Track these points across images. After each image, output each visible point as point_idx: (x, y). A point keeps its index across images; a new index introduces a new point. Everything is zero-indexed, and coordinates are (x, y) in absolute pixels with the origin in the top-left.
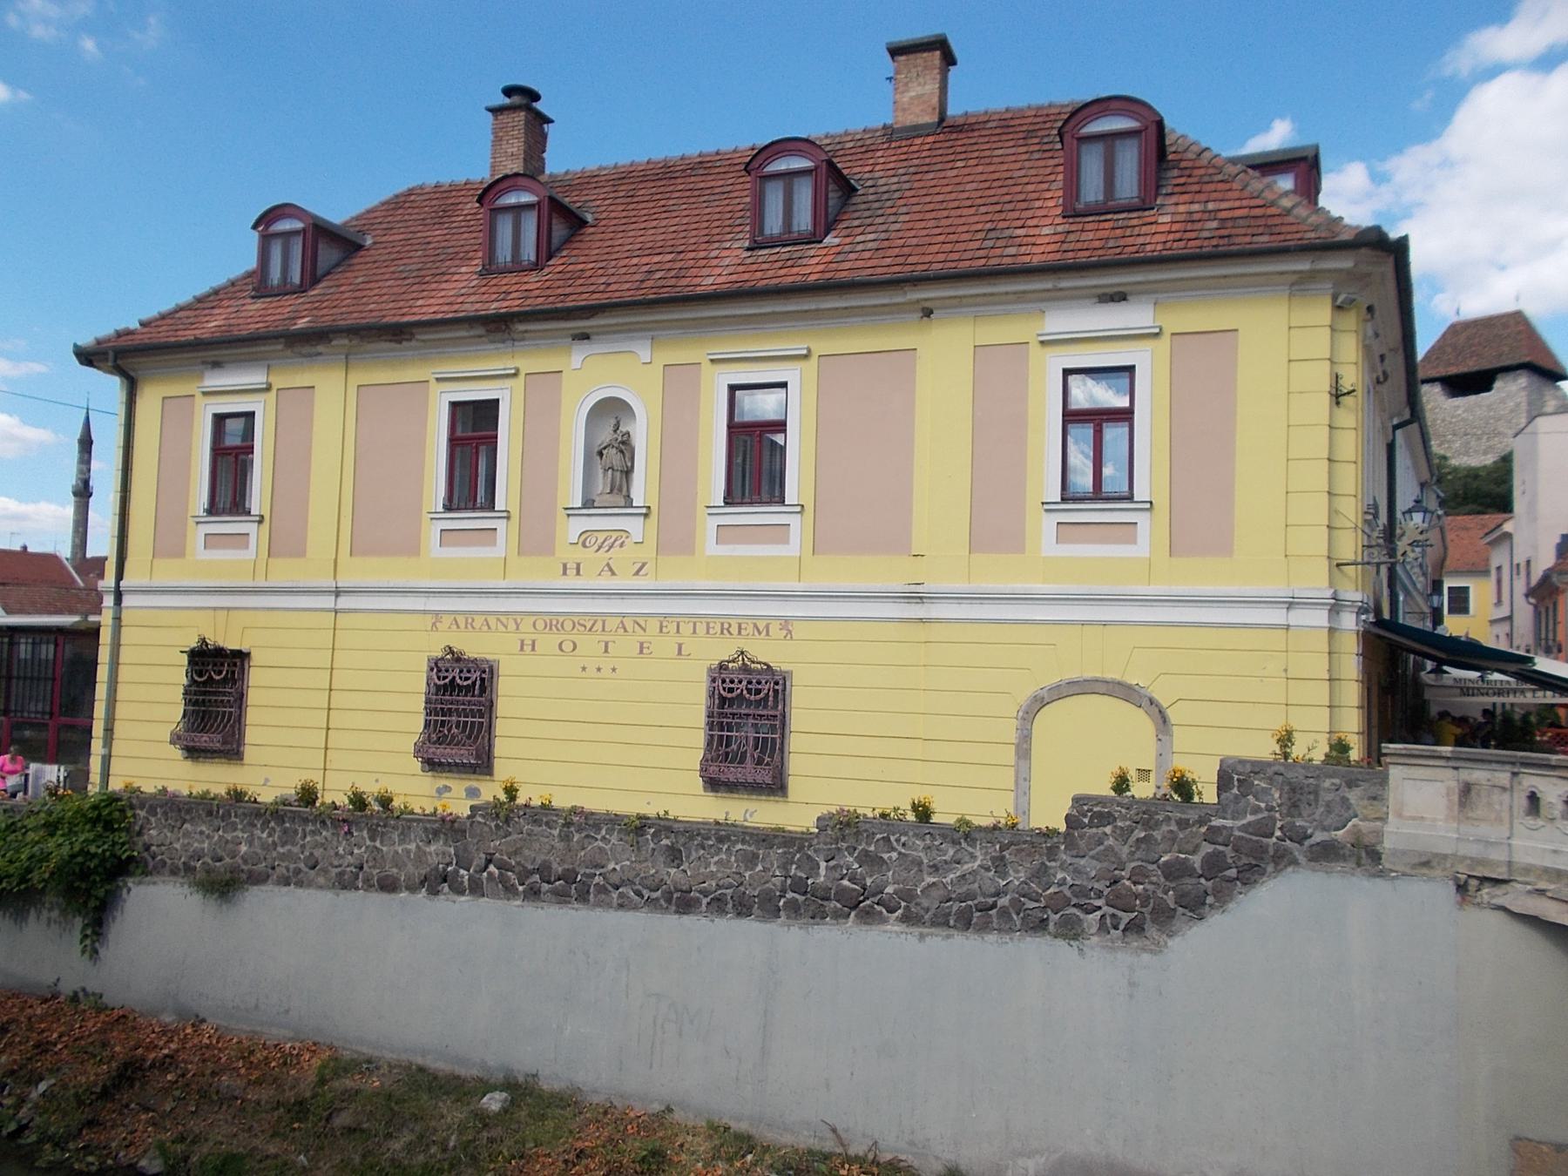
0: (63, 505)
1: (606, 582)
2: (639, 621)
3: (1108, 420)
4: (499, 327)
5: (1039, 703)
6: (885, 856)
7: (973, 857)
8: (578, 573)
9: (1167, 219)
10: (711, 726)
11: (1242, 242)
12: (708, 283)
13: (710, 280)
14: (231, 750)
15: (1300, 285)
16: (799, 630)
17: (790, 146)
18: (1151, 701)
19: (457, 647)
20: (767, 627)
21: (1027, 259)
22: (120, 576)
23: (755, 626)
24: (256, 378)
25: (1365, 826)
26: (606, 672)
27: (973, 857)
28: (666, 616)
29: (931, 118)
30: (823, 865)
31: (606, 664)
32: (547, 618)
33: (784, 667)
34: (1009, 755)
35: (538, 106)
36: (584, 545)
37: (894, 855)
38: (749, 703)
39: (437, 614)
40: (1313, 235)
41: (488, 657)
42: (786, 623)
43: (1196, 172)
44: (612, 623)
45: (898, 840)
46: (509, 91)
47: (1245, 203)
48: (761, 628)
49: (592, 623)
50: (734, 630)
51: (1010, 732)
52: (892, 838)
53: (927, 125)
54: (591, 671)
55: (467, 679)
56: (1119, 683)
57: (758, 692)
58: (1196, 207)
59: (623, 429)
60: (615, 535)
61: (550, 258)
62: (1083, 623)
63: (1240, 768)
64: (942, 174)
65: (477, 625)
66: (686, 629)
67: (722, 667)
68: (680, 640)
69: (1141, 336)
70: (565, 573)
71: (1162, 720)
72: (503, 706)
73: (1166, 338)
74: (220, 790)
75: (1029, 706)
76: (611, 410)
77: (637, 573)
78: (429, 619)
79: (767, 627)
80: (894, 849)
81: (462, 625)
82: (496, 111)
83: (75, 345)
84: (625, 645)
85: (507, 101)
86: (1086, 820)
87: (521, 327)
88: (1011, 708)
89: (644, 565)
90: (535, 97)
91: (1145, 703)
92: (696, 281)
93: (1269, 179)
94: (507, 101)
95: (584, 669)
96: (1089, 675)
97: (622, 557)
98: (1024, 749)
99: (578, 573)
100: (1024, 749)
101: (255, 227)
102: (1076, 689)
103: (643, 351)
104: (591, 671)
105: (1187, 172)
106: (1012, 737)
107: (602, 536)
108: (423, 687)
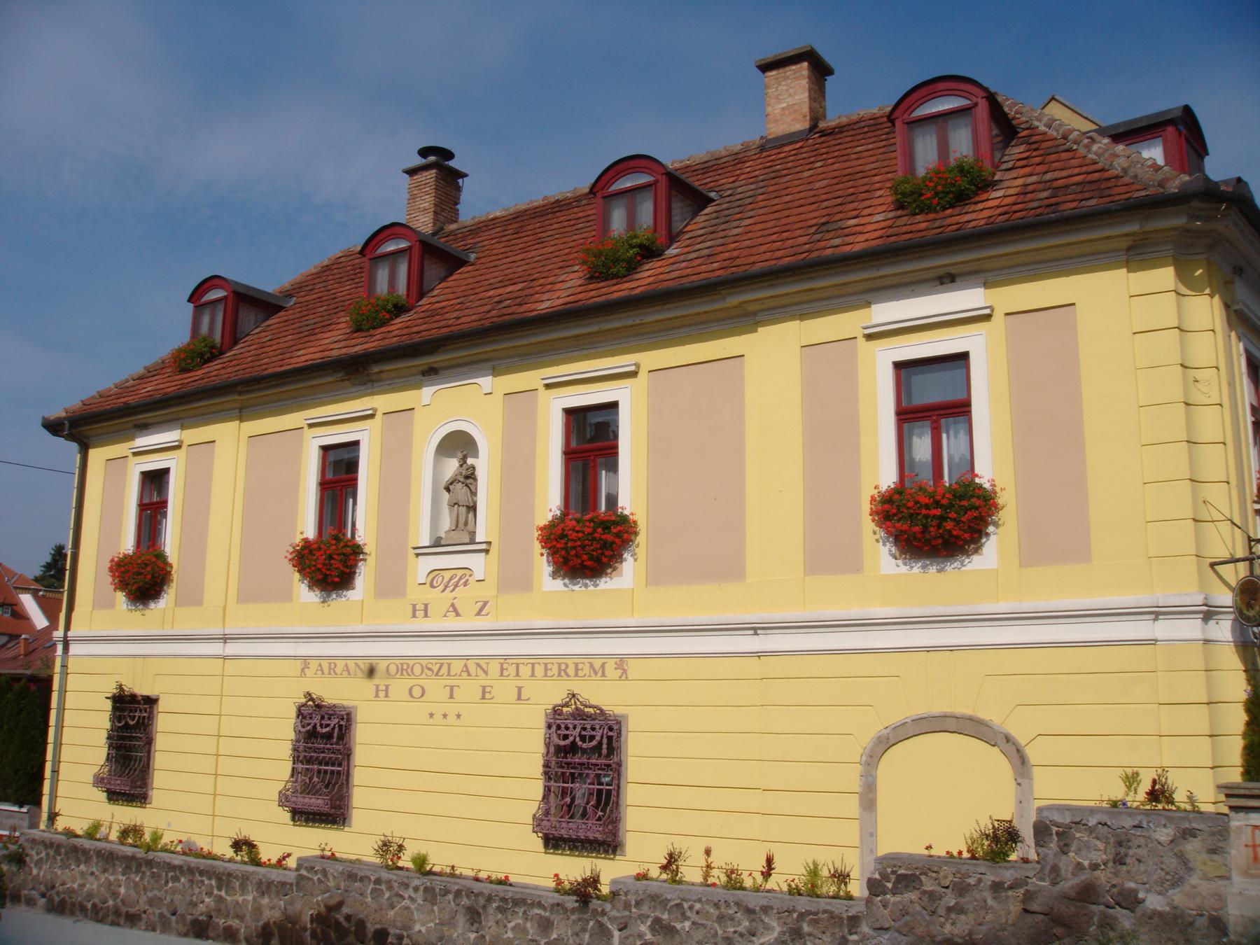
0: (287, 596)
1: (452, 624)
2: (481, 663)
3: (947, 416)
4: (357, 371)
5: (885, 743)
6: (678, 926)
7: (768, 928)
8: (426, 615)
9: (1000, 193)
10: (296, 759)
11: (1068, 207)
12: (545, 305)
13: (547, 304)
14: (334, 813)
15: (1137, 255)
16: (633, 667)
17: (632, 163)
18: (1008, 739)
19: (317, 692)
20: (603, 666)
21: (847, 249)
22: (67, 628)
23: (591, 665)
24: (968, 298)
25: (1205, 888)
26: (452, 718)
27: (768, 928)
28: (506, 657)
29: (802, 125)
30: (616, 934)
31: (452, 709)
32: (398, 662)
33: (618, 711)
34: (852, 806)
35: (452, 163)
36: (432, 586)
37: (687, 924)
38: (584, 751)
39: (305, 659)
40: (1143, 193)
41: (345, 703)
42: (621, 661)
43: (1044, 145)
44: (457, 666)
45: (691, 908)
46: (424, 152)
47: (1084, 169)
48: (596, 667)
49: (438, 666)
50: (571, 671)
51: (852, 778)
52: (686, 905)
53: (800, 132)
54: (438, 718)
55: (327, 725)
56: (971, 719)
57: (592, 738)
58: (1034, 179)
59: (470, 461)
60: (460, 573)
61: (421, 296)
62: (929, 649)
63: (1057, 818)
64: (799, 176)
65: (338, 670)
66: (525, 671)
67: (556, 711)
68: (519, 683)
69: (978, 322)
70: (414, 616)
71: (1020, 761)
72: (161, 742)
73: (998, 320)
74: (129, 854)
75: (872, 750)
76: (458, 444)
77: (479, 613)
78: (298, 664)
79: (603, 666)
80: (688, 918)
81: (326, 670)
82: (411, 172)
83: (44, 418)
84: (469, 689)
85: (424, 161)
86: (890, 885)
87: (376, 369)
88: (855, 750)
89: (485, 603)
90: (447, 155)
91: (1002, 741)
92: (534, 306)
93: (1133, 148)
94: (424, 161)
95: (431, 715)
96: (937, 710)
97: (466, 596)
98: (868, 799)
99: (426, 615)
100: (868, 799)
101: (189, 300)
102: (951, 724)
103: (486, 382)
104: (438, 718)
105: (1034, 146)
106: (855, 784)
107: (447, 575)
108: (541, 748)
